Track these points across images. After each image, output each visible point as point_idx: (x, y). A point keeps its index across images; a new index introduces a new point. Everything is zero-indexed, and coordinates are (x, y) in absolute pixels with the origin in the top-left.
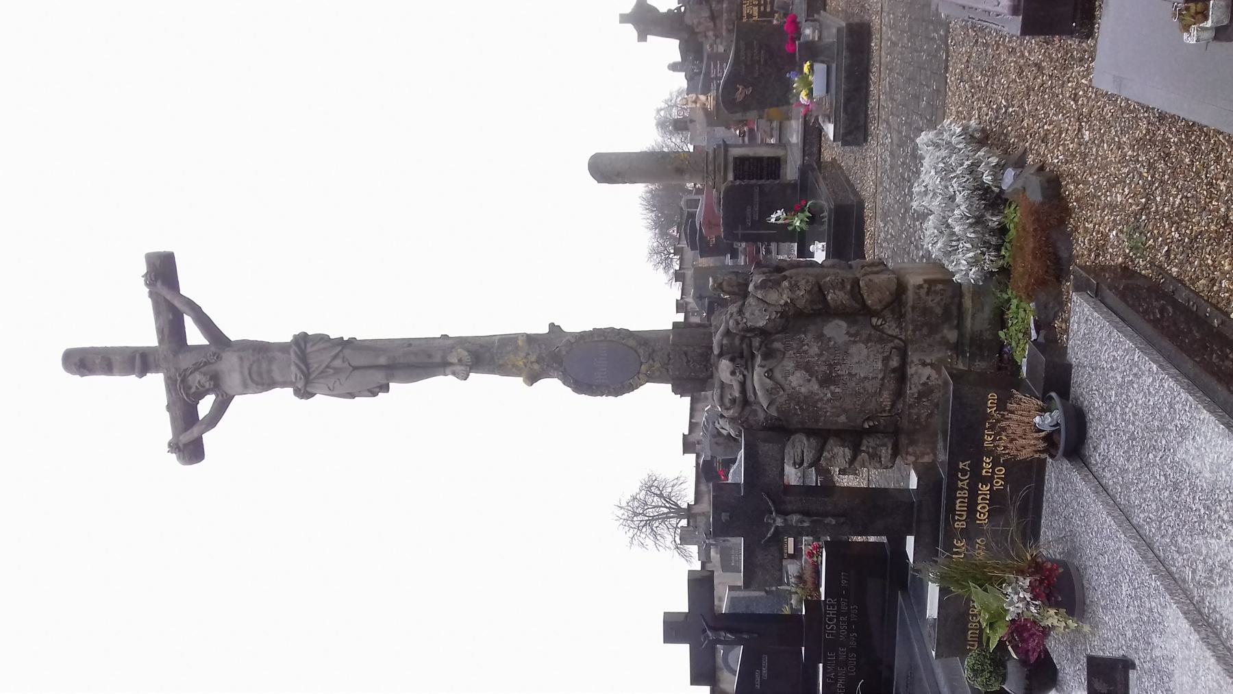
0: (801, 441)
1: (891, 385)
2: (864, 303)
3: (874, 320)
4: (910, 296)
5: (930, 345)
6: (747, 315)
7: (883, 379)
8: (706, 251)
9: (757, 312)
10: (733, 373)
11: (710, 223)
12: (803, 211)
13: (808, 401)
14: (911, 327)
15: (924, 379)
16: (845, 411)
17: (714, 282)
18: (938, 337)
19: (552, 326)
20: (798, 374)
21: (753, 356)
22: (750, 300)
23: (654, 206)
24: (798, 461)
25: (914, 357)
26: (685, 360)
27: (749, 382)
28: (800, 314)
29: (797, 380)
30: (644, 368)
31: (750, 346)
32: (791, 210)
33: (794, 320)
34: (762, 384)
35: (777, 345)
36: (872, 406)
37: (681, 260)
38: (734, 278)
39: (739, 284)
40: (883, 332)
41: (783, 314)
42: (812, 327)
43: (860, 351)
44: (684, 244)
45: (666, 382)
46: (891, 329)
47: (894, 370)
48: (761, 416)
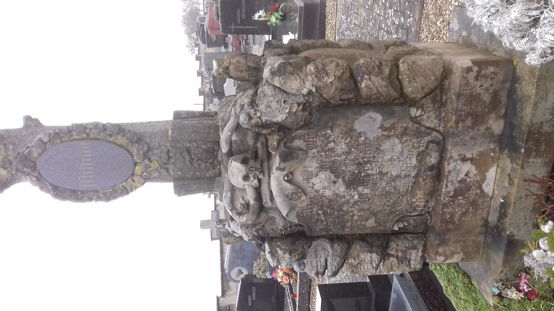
0: (324, 249)
1: (426, 184)
2: (402, 93)
3: (414, 112)
4: (456, 80)
5: (472, 138)
6: (262, 107)
7: (417, 176)
8: (211, 44)
9: (274, 105)
10: (246, 178)
11: (212, 27)
12: (277, 11)
13: (331, 205)
14: (454, 118)
15: (462, 176)
16: (374, 214)
17: (219, 65)
18: (482, 128)
19: (28, 119)
20: (322, 175)
21: (269, 156)
22: (265, 89)
23: (184, 23)
24: (321, 270)
25: (453, 152)
26: (187, 158)
27: (264, 187)
28: (326, 106)
29: (321, 183)
30: (138, 169)
31: (266, 145)
32: (270, 11)
33: (320, 112)
34: (282, 190)
35: (298, 143)
36: (403, 206)
37: (199, 50)
38: (243, 61)
39: (249, 69)
40: (420, 124)
41: (305, 106)
42: (341, 122)
43: (393, 147)
44: (199, 42)
45: (169, 181)
46: (430, 120)
47: (431, 168)
48: (280, 224)
